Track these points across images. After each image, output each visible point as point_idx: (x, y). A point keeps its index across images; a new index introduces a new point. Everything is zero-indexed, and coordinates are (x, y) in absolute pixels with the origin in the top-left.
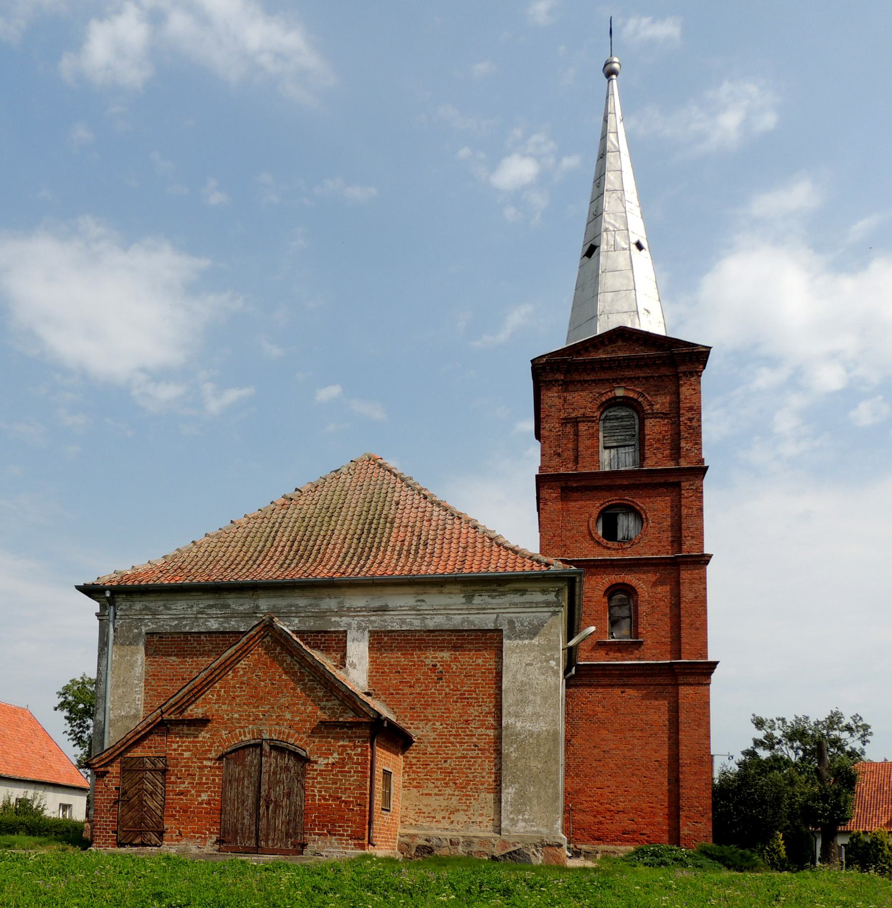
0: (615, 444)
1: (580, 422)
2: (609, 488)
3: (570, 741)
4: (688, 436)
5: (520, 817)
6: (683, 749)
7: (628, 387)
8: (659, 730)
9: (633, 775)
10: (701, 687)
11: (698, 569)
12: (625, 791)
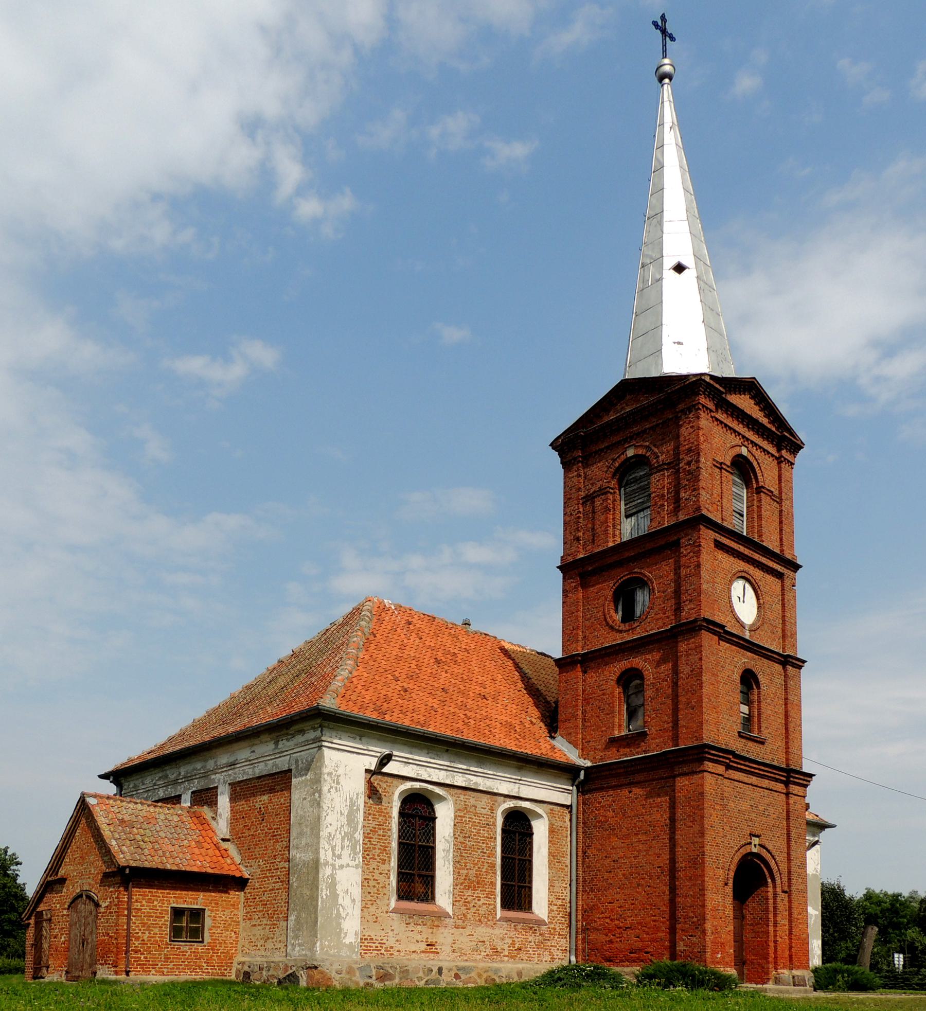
0: (634, 510)
1: (596, 497)
2: (620, 564)
3: (585, 853)
4: (687, 483)
5: (297, 942)
6: (678, 851)
7: (637, 444)
8: (661, 831)
9: (639, 885)
10: (695, 776)
11: (693, 638)
12: (632, 904)
